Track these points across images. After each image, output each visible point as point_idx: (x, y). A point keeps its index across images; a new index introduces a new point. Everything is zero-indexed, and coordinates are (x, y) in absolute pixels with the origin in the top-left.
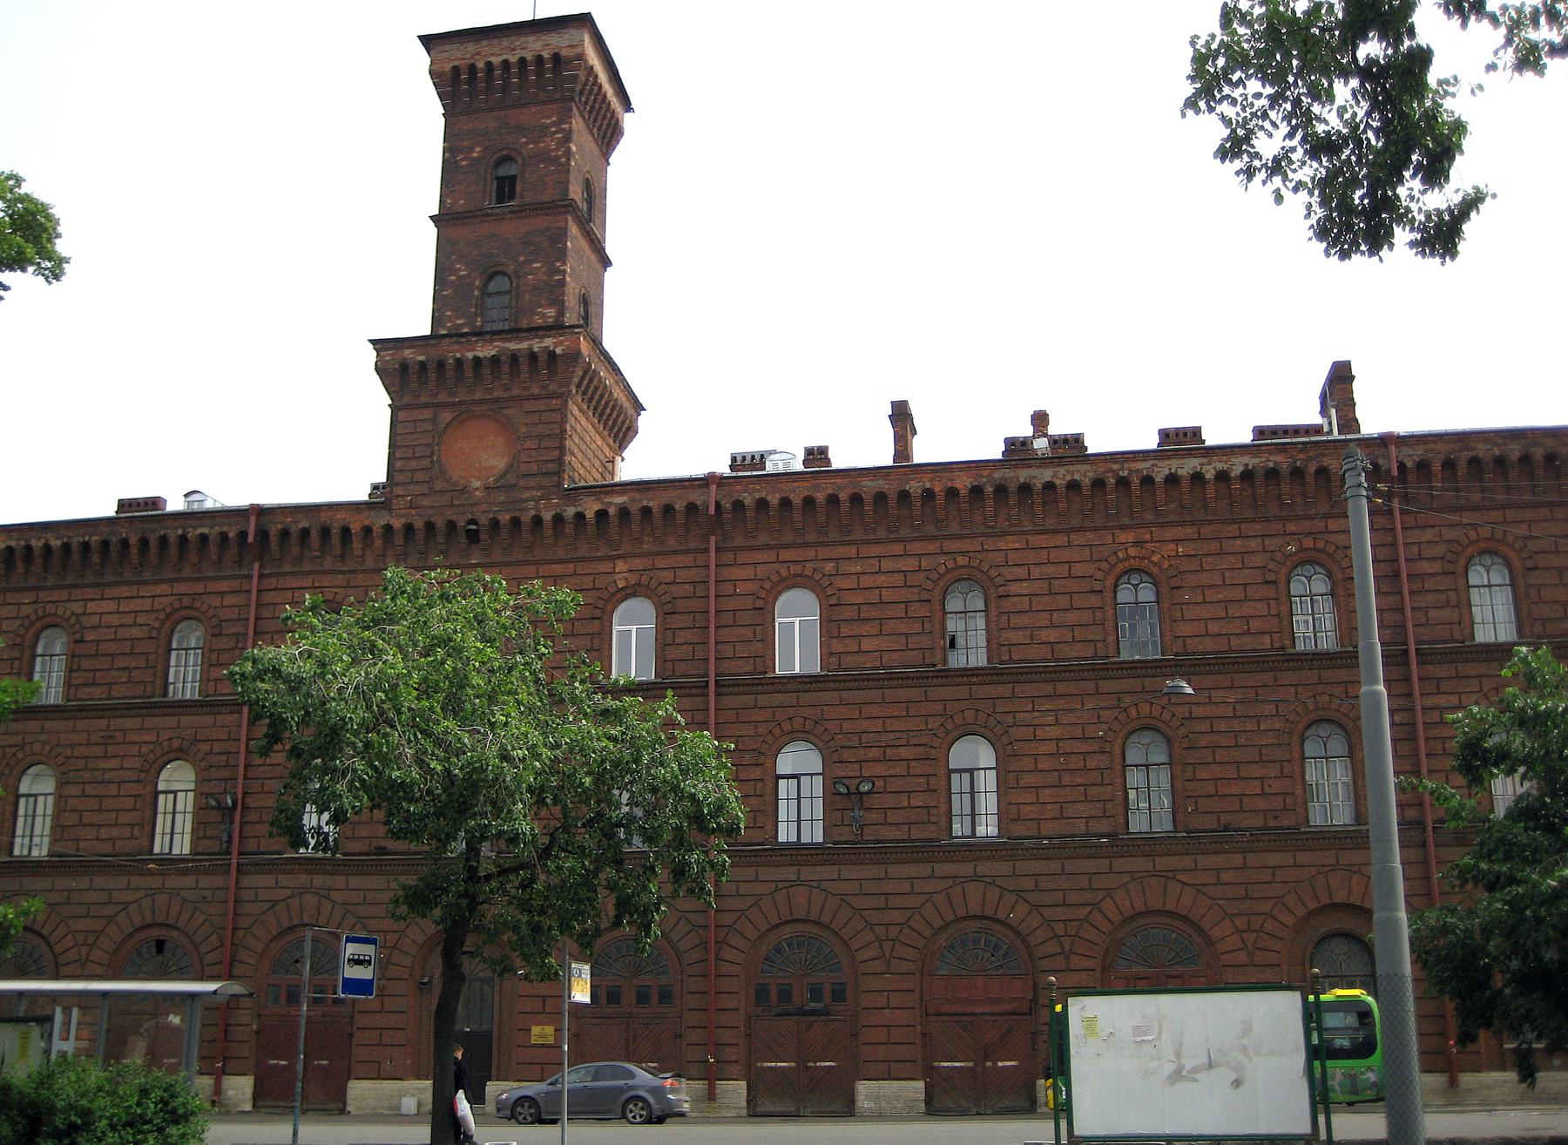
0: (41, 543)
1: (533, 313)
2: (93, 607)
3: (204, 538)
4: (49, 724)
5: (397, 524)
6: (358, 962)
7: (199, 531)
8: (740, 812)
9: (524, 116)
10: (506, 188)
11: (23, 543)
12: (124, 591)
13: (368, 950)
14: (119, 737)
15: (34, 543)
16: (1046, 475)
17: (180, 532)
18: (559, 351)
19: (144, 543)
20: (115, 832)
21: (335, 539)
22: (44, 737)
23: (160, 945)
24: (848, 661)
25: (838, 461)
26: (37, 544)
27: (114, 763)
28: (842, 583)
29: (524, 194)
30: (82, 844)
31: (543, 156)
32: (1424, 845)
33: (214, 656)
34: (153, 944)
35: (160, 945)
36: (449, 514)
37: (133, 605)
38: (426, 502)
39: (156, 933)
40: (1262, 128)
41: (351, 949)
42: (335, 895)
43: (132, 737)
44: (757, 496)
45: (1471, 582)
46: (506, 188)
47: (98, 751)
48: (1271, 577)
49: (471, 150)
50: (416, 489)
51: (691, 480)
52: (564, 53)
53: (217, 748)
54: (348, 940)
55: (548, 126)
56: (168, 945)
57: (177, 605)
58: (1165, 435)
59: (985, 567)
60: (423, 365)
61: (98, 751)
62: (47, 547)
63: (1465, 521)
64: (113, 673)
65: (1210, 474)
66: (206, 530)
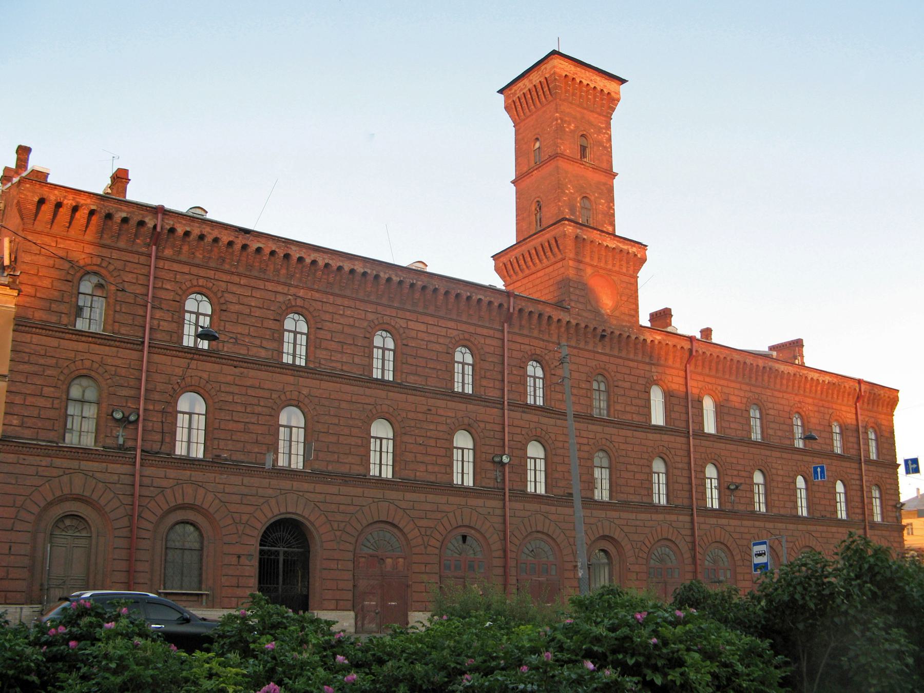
0: (387, 276)
2: (411, 325)
3: (479, 301)
4: (391, 394)
5: (574, 322)
6: (760, 555)
7: (479, 297)
11: (375, 273)
13: (763, 548)
14: (434, 410)
15: (382, 274)
17: (469, 294)
19: (447, 293)
20: (436, 469)
21: (545, 321)
22: (387, 402)
23: (464, 538)
24: (727, 431)
25: (715, 339)
26: (384, 276)
27: (432, 427)
28: (228, 297)
30: (418, 474)
31: (600, 143)
32: (692, 515)
33: (483, 372)
34: (460, 538)
35: (464, 538)
39: (464, 531)
41: (757, 549)
42: (550, 517)
43: (441, 412)
44: (326, 261)
45: (81, 290)
47: (421, 416)
48: (69, 278)
52: (613, 94)
53: (488, 427)
54: (755, 544)
56: (468, 538)
57: (461, 337)
59: (311, 309)
61: (421, 416)
62: (389, 280)
63: (242, 282)
64: (427, 370)
65: (321, 263)
66: (483, 298)
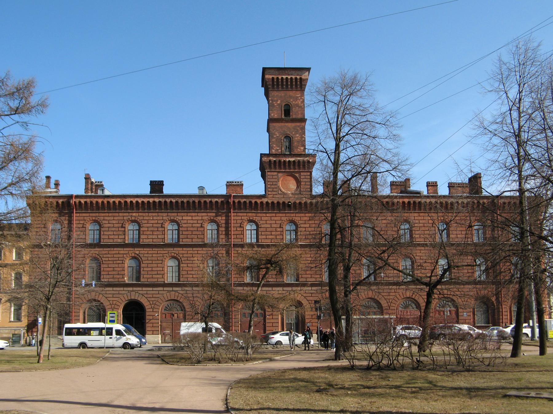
1: (297, 148)
8: (260, 350)
9: (291, 93)
10: (287, 112)
12: (193, 214)
16: (428, 200)
18: (311, 161)
29: (293, 115)
31: (297, 105)
36: (283, 200)
37: (197, 218)
38: (277, 196)
40: (448, 304)
46: (287, 112)
49: (277, 101)
50: (274, 193)
51: (85, 186)
55: (298, 97)
58: (262, 87)
60: (275, 161)
